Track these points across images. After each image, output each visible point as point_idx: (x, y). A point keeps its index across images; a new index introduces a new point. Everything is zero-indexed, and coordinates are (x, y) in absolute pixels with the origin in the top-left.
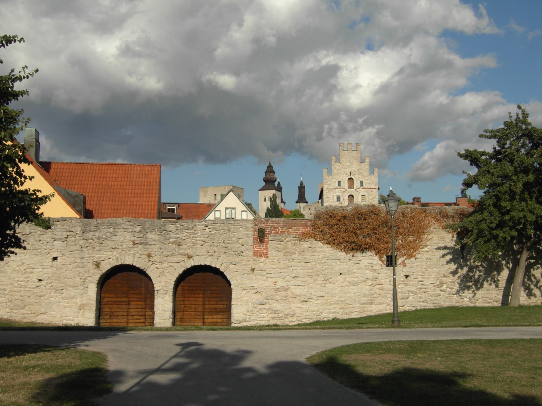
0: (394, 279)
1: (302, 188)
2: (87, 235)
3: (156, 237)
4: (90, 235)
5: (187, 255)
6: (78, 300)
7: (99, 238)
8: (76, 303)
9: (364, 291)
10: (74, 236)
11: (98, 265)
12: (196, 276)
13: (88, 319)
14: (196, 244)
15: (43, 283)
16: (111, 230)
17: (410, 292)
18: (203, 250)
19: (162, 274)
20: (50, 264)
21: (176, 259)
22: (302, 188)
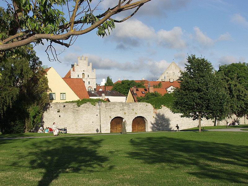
0: (100, 125)
1: (88, 75)
2: (107, 108)
3: (127, 108)
4: (108, 107)
5: (135, 113)
6: (105, 128)
7: (110, 108)
8: (105, 129)
9: (180, 123)
10: (103, 108)
11: (110, 117)
12: (138, 118)
13: (131, 132)
14: (138, 110)
15: (94, 123)
16: (114, 106)
17: (191, 123)
18: (140, 112)
19: (129, 119)
20: (96, 117)
21: (133, 114)
22: (88, 75)
